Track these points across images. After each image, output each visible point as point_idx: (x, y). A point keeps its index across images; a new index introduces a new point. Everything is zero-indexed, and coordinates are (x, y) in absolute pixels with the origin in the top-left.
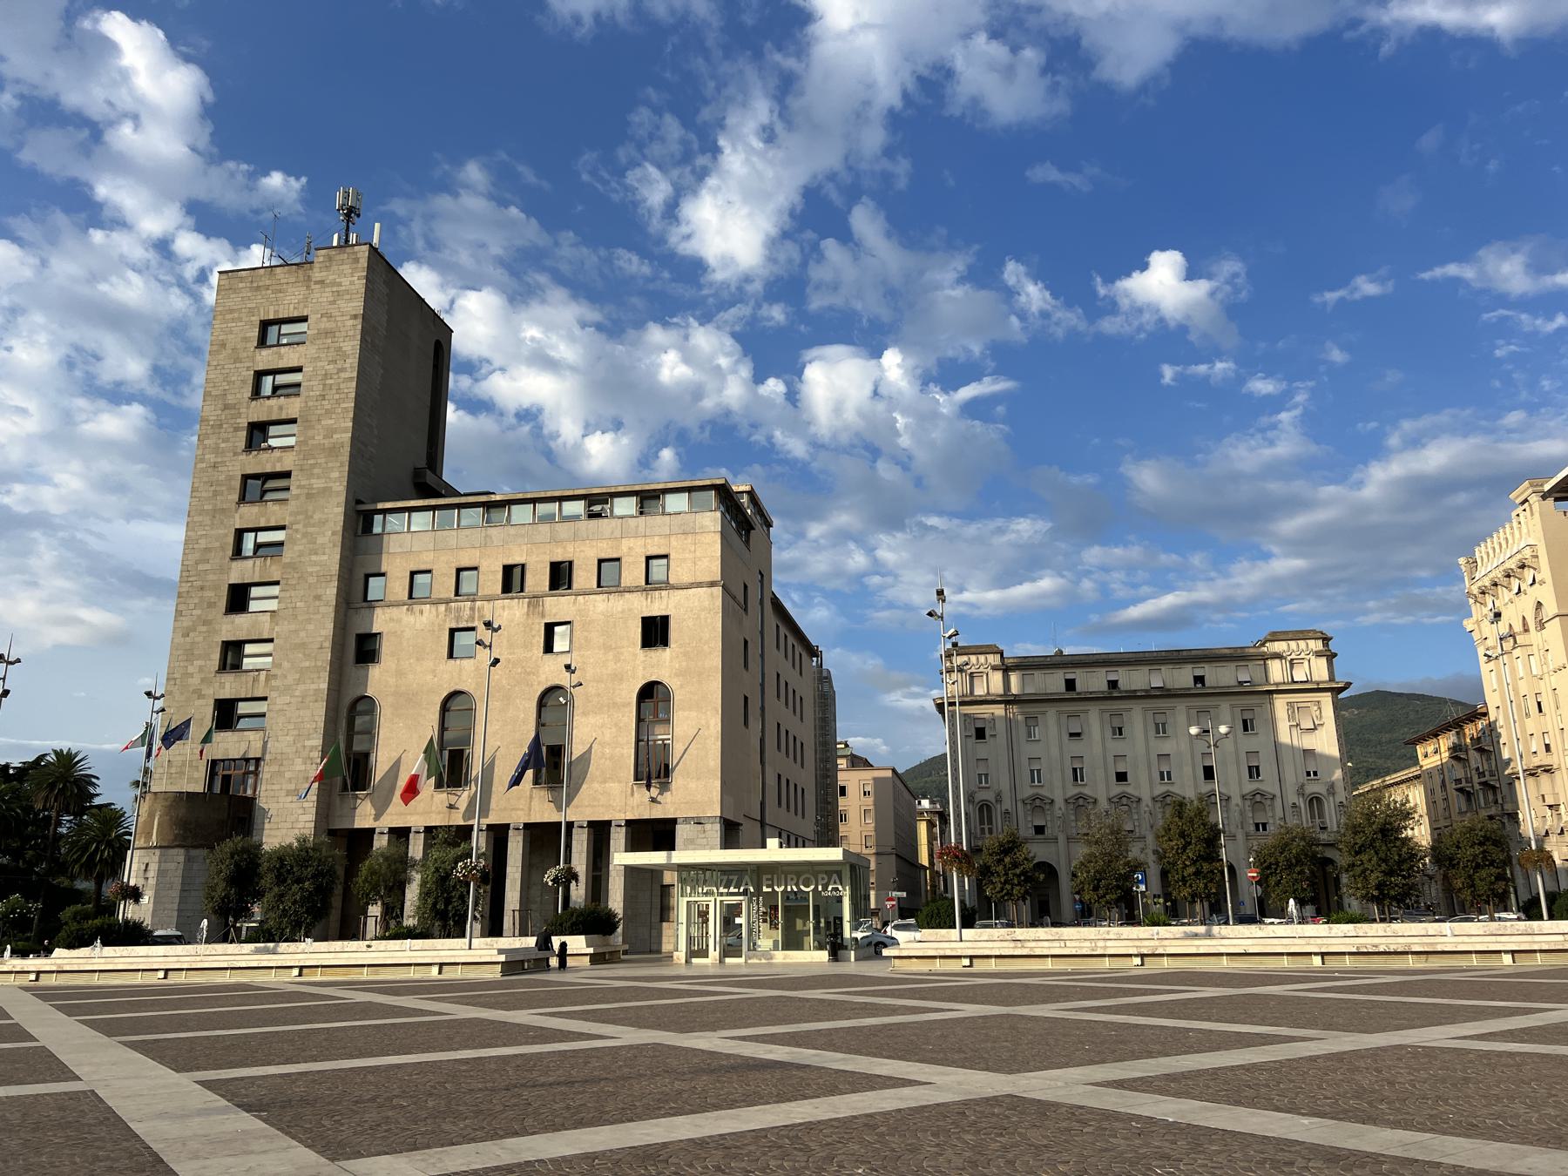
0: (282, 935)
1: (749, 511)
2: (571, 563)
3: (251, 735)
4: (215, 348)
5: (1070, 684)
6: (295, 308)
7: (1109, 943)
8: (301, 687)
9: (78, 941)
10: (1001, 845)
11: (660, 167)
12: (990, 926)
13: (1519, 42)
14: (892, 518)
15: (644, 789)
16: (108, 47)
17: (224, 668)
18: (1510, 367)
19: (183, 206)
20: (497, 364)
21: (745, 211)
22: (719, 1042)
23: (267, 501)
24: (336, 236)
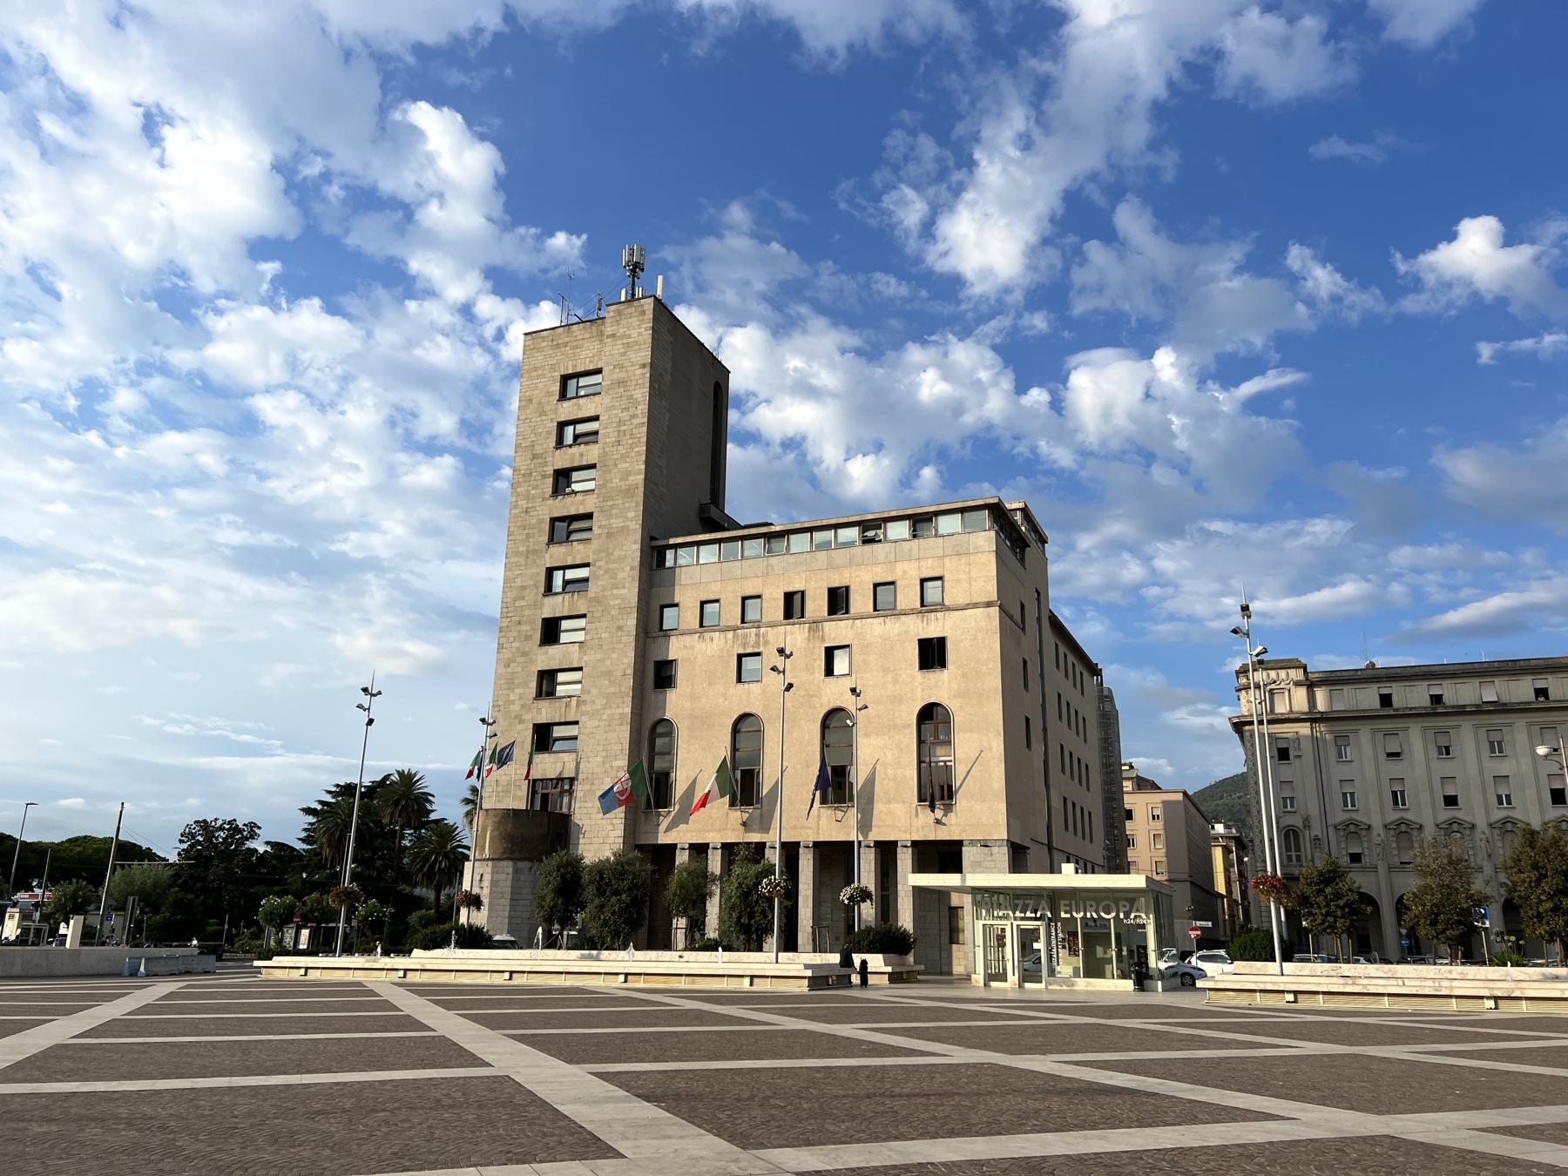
0: (603, 943)
1: (1023, 528)
2: (847, 588)
3: (566, 757)
5: (1386, 700)
7: (1455, 984)
8: (608, 712)
9: (435, 942)
10: (1321, 874)
11: (915, 187)
12: (1308, 960)
14: (1170, 525)
15: (928, 810)
16: (416, 134)
17: (541, 696)
19: (482, 272)
20: (762, 396)
21: (1002, 222)
22: (1053, 1065)
23: (572, 541)
24: (623, 291)
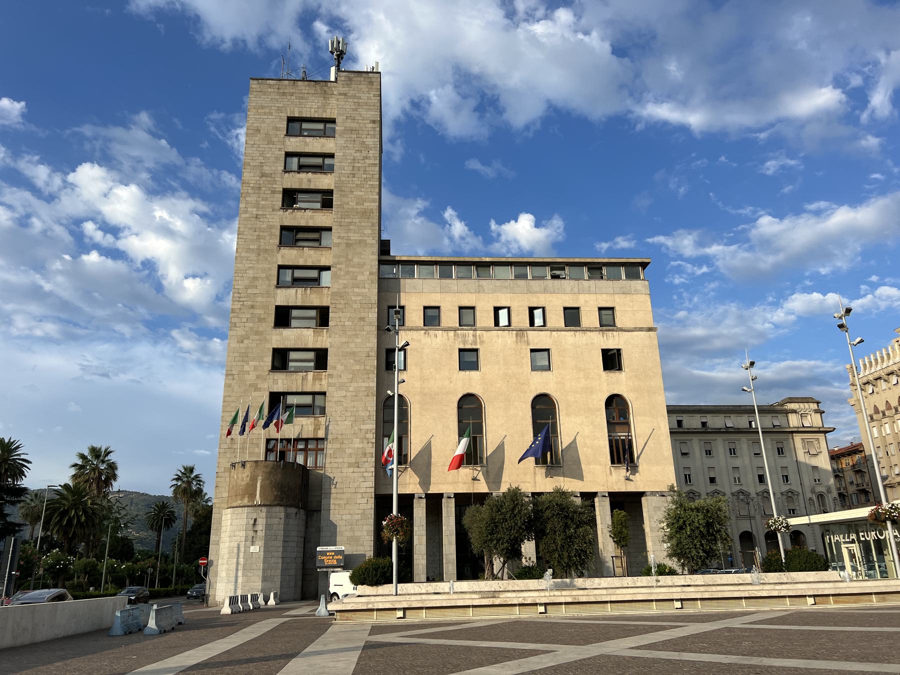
4: (251, 132)
6: (315, 112)
8: (354, 385)
13: (702, 132)
18: (682, 290)
20: (135, 230)
